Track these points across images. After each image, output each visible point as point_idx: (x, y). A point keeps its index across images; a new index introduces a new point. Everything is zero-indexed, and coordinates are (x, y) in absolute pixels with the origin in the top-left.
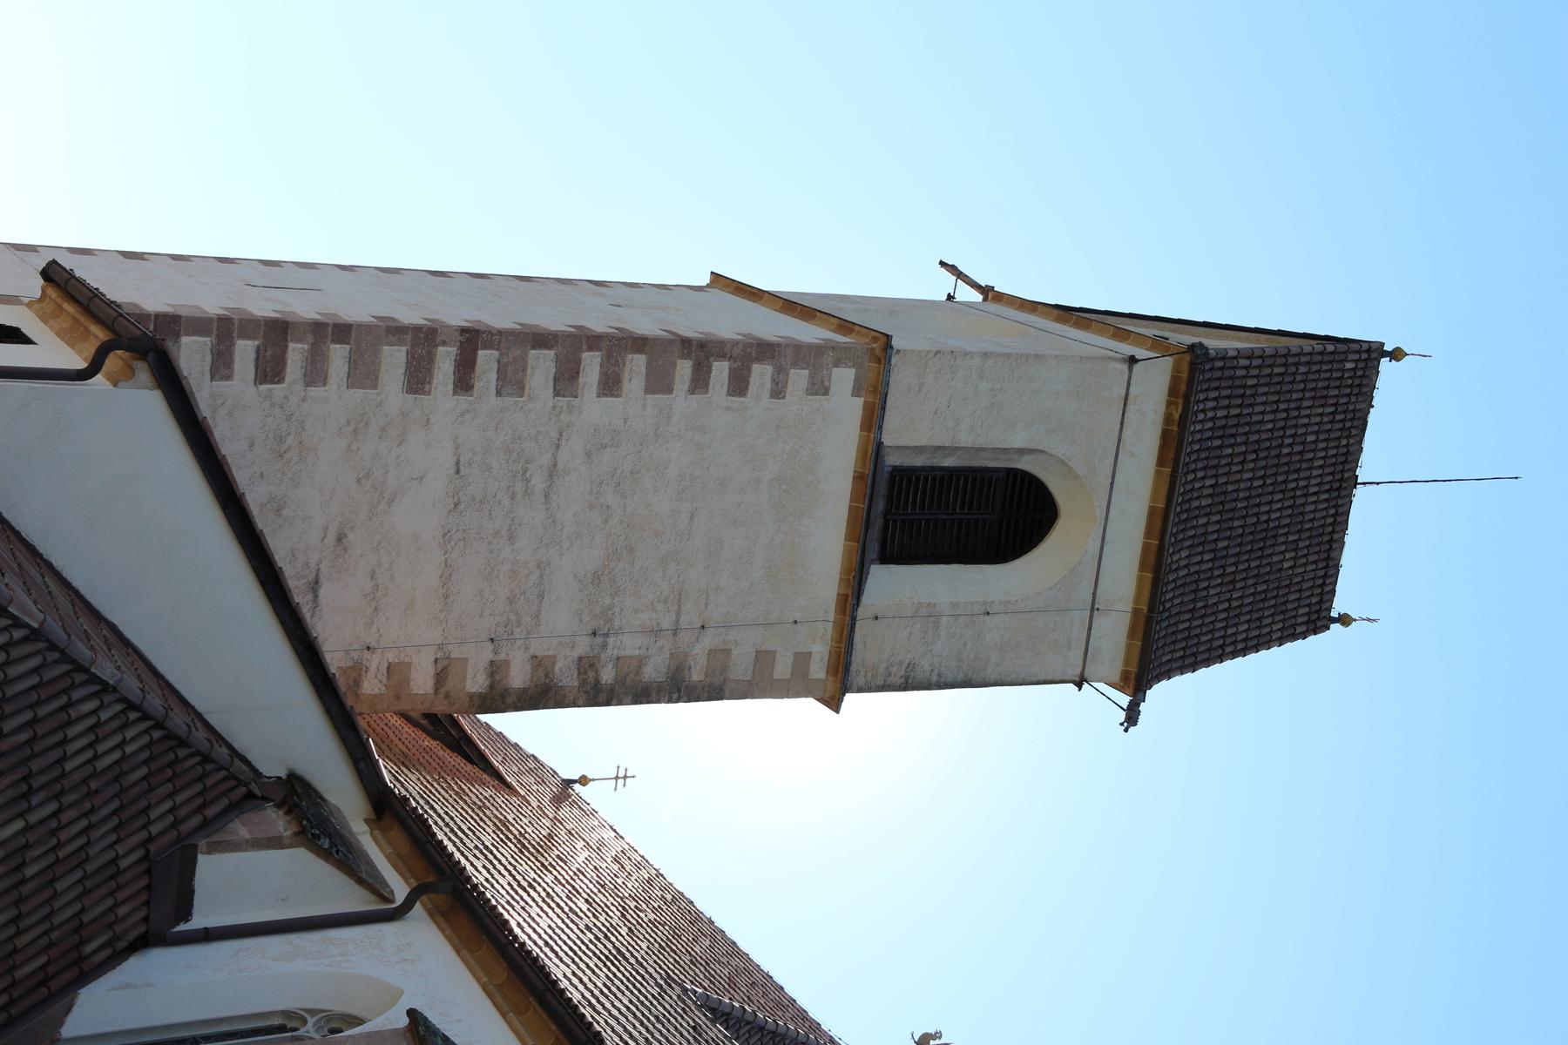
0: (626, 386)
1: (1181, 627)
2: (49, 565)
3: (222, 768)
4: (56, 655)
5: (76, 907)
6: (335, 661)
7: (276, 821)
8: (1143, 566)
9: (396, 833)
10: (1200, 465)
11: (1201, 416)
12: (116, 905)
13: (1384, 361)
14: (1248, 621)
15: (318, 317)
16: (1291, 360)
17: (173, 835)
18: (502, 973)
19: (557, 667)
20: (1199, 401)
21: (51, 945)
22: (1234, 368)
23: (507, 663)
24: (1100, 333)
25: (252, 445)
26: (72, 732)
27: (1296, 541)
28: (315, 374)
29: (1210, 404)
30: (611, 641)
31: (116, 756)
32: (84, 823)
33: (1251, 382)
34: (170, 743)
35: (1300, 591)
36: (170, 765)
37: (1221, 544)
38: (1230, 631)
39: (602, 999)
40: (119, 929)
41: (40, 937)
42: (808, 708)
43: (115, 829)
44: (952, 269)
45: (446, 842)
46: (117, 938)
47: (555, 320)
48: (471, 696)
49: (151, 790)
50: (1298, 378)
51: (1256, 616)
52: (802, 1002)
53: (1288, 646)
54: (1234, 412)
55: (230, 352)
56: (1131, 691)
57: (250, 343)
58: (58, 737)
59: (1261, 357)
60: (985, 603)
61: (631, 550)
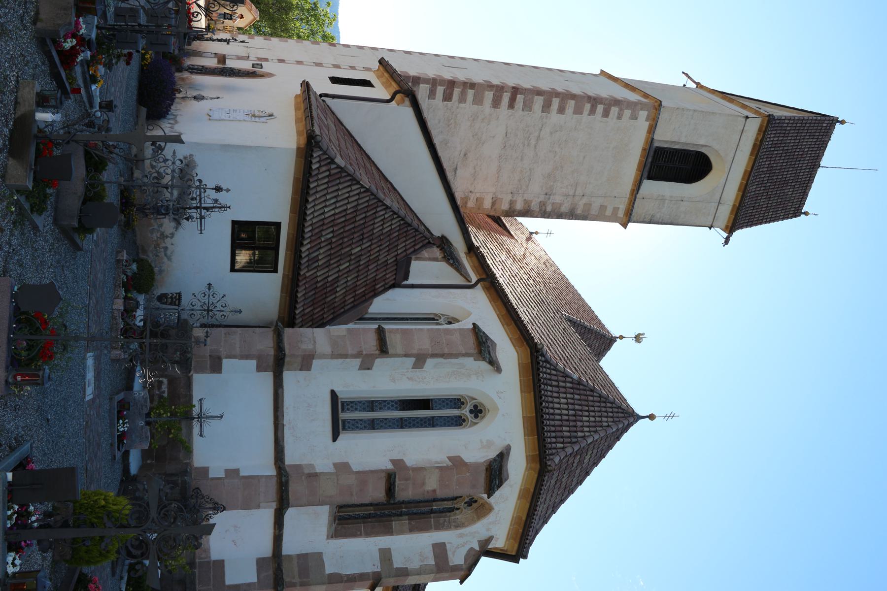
0: (567, 111)
1: (749, 212)
2: (373, 162)
3: (421, 234)
4: (373, 197)
5: (375, 274)
6: (458, 196)
7: (436, 252)
8: (739, 190)
9: (474, 258)
10: (765, 157)
11: (768, 140)
12: (386, 274)
13: (838, 124)
14: (772, 212)
15: (465, 80)
16: (804, 122)
17: (404, 254)
18: (504, 312)
19: (532, 204)
20: (769, 134)
21: (367, 285)
22: (783, 123)
23: (516, 201)
24: (736, 105)
25: (439, 122)
26: (376, 221)
27: (794, 185)
28: (462, 99)
29: (772, 136)
30: (551, 197)
31: (389, 228)
32: (378, 249)
33: (788, 128)
34: (406, 225)
35: (793, 202)
36: (405, 232)
37: (768, 185)
38: (766, 215)
39: (535, 320)
40: (386, 281)
41: (364, 282)
42: (617, 226)
43: (387, 251)
44: (687, 75)
45: (490, 265)
46: (386, 284)
47: (545, 86)
48: (503, 211)
49: (399, 239)
50: (806, 128)
51: (776, 210)
52: (600, 317)
53: (785, 221)
54: (780, 139)
55: (435, 90)
56: (728, 232)
57: (442, 87)
58: (372, 222)
59: (793, 120)
60: (682, 197)
61: (562, 167)
